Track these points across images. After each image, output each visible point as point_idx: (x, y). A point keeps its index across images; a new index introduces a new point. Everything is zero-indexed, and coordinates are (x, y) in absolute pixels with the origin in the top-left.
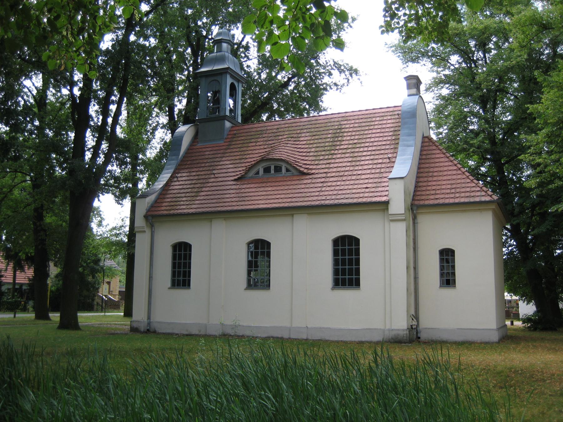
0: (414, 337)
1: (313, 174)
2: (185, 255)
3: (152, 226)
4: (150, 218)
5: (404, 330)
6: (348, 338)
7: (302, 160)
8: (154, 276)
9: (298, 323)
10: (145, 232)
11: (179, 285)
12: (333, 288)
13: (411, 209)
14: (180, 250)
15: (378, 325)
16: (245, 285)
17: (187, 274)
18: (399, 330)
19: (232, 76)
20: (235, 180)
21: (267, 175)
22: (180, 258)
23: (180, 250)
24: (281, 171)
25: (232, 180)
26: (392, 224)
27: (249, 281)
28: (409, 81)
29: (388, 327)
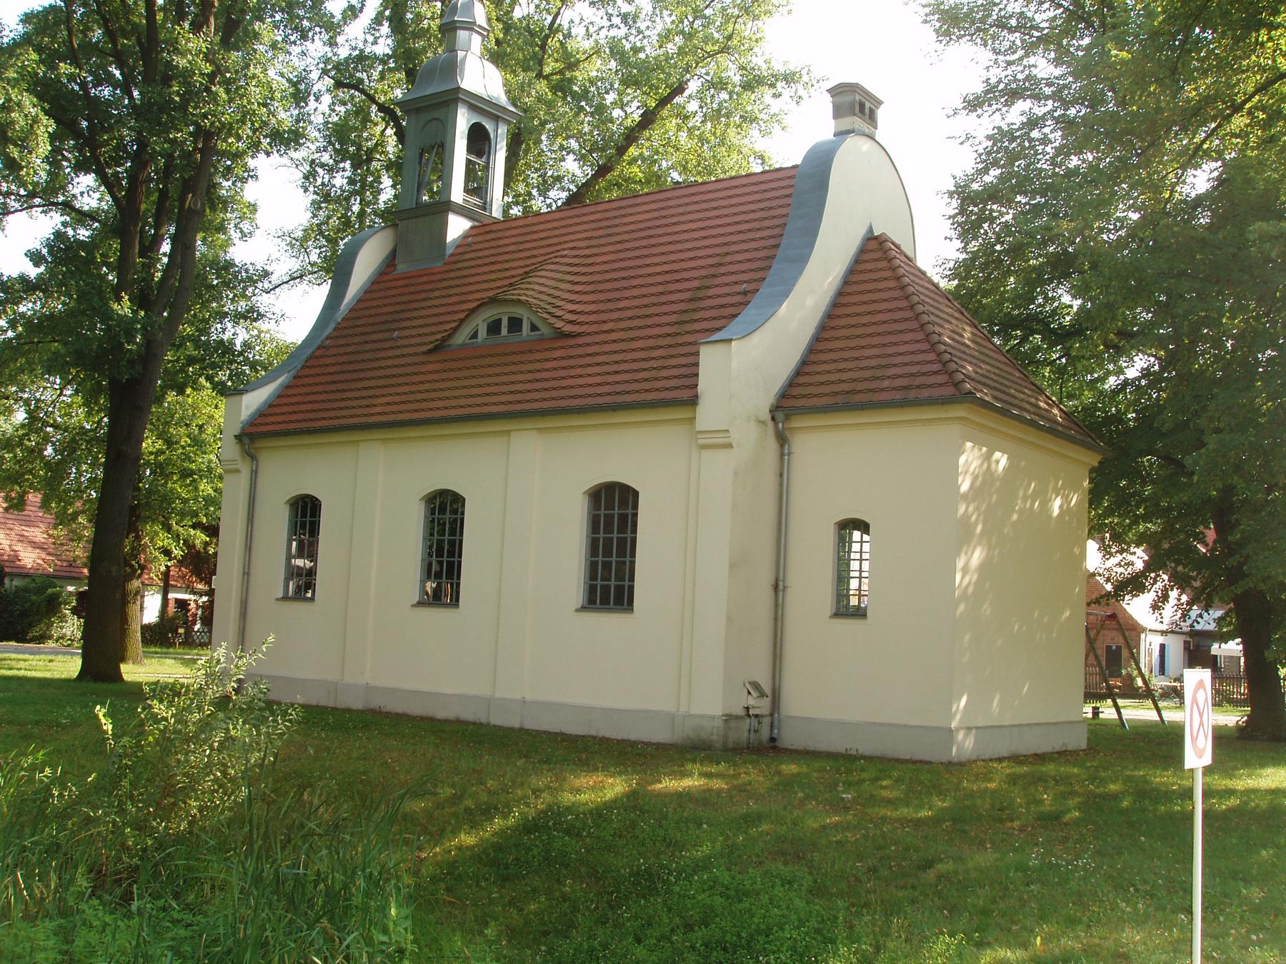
0: (756, 741)
1: (579, 335)
2: (623, 518)
3: (251, 456)
4: (246, 440)
5: (713, 717)
6: (442, 713)
7: (571, 301)
8: (253, 571)
9: (506, 691)
10: (237, 471)
11: (605, 601)
12: (583, 608)
13: (773, 419)
14: (610, 506)
15: (662, 702)
16: (828, 605)
17: (626, 572)
18: (702, 716)
19: (472, 108)
20: (430, 352)
21: (496, 339)
22: (609, 528)
23: (610, 506)
24: (520, 330)
25: (424, 353)
26: (707, 454)
27: (591, 591)
28: (840, 99)
29: (683, 709)
